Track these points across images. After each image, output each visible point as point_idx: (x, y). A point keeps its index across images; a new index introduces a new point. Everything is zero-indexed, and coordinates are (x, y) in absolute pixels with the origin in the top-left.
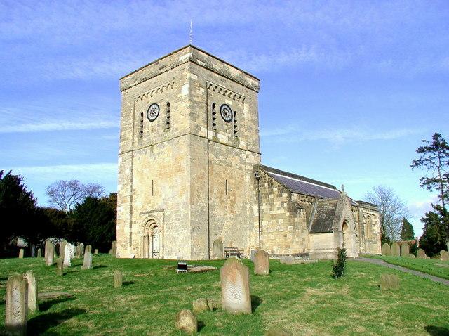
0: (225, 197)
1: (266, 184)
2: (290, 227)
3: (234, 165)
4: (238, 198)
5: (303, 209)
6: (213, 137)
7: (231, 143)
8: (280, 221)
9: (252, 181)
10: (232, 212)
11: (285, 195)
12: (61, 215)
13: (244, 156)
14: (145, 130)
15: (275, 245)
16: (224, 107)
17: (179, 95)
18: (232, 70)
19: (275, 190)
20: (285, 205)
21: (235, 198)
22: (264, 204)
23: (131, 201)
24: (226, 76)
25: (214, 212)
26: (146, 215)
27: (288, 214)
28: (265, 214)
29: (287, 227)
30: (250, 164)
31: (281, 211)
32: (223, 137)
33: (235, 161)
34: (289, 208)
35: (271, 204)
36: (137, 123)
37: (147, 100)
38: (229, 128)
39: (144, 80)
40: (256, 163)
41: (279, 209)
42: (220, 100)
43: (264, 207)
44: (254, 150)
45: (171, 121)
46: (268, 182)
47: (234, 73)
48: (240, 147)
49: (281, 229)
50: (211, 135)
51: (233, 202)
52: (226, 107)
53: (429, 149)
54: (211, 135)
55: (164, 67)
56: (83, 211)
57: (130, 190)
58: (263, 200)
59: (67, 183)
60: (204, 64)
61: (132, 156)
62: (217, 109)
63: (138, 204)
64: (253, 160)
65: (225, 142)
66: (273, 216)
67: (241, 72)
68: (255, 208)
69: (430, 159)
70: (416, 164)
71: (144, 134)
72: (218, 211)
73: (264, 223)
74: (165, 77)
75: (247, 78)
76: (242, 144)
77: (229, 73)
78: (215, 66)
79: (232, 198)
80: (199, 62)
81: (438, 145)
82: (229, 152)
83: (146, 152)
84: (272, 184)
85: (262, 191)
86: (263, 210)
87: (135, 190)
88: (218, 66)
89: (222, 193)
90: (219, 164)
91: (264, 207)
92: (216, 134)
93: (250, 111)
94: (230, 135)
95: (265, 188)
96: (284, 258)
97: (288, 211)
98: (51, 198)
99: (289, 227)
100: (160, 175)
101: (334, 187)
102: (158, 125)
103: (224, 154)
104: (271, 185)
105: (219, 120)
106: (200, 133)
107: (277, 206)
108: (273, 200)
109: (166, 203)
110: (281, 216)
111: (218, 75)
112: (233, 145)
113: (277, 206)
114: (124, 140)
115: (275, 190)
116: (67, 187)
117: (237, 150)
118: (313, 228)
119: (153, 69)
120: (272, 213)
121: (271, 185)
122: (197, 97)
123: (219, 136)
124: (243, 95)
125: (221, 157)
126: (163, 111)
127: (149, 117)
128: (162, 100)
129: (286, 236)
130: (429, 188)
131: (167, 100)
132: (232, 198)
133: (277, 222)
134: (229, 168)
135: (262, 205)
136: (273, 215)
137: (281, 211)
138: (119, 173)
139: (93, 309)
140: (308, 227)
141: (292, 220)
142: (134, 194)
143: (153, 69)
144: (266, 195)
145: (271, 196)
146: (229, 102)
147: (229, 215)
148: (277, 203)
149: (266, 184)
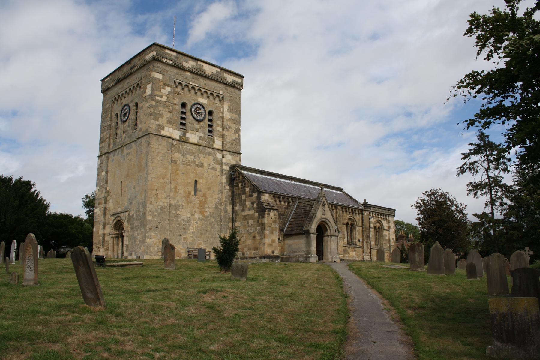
0: (193, 197)
1: (240, 184)
2: (259, 228)
3: (205, 164)
4: (210, 199)
5: (274, 210)
6: (180, 137)
7: (203, 143)
8: (251, 222)
9: (227, 181)
10: (202, 213)
11: (255, 195)
14: (119, 132)
15: (246, 247)
17: (144, 95)
18: (206, 67)
19: (247, 190)
20: (255, 205)
21: (206, 198)
22: (238, 205)
23: (105, 203)
24: (199, 74)
25: (178, 212)
26: (115, 217)
27: (257, 215)
28: (238, 215)
29: (256, 229)
30: (227, 164)
31: (251, 212)
32: (193, 137)
33: (207, 161)
34: (258, 208)
35: (243, 205)
36: (113, 124)
38: (201, 127)
40: (234, 163)
41: (250, 209)
42: (190, 98)
43: (237, 208)
44: (233, 150)
45: (138, 122)
46: (241, 182)
47: (209, 70)
48: (215, 146)
49: (251, 230)
50: (177, 134)
51: (203, 204)
53: (476, 152)
54: (177, 134)
55: (134, 66)
57: (104, 192)
58: (237, 201)
60: (171, 62)
61: (108, 159)
62: (188, 107)
63: (111, 205)
64: (230, 159)
65: (196, 141)
66: (246, 218)
67: (219, 70)
68: (229, 208)
70: (462, 170)
71: (119, 135)
72: (183, 211)
75: (226, 75)
76: (218, 144)
77: (204, 71)
78: (185, 64)
82: (202, 152)
83: (118, 153)
84: (245, 184)
85: (237, 192)
86: (237, 211)
87: (109, 192)
88: (190, 64)
89: (189, 193)
90: (186, 164)
92: (184, 134)
93: (230, 110)
94: (202, 135)
95: (238, 189)
96: (329, 251)
97: (257, 212)
99: (258, 228)
100: (128, 175)
101: (340, 189)
102: (129, 126)
103: (193, 154)
106: (163, 133)
107: (248, 206)
108: (245, 201)
109: (131, 203)
110: (251, 217)
111: (188, 74)
112: (206, 146)
113: (248, 206)
115: (247, 190)
117: (211, 150)
121: (244, 187)
122: (162, 97)
123: (188, 135)
124: (221, 93)
125: (190, 157)
126: (133, 108)
129: (254, 237)
131: (136, 100)
133: (248, 223)
134: (199, 168)
135: (236, 206)
136: (245, 216)
137: (251, 212)
139: (16, 323)
140: (282, 230)
141: (260, 220)
142: (108, 195)
144: (240, 195)
145: (244, 197)
146: (203, 100)
147: (197, 215)
148: (248, 204)
149: (240, 184)
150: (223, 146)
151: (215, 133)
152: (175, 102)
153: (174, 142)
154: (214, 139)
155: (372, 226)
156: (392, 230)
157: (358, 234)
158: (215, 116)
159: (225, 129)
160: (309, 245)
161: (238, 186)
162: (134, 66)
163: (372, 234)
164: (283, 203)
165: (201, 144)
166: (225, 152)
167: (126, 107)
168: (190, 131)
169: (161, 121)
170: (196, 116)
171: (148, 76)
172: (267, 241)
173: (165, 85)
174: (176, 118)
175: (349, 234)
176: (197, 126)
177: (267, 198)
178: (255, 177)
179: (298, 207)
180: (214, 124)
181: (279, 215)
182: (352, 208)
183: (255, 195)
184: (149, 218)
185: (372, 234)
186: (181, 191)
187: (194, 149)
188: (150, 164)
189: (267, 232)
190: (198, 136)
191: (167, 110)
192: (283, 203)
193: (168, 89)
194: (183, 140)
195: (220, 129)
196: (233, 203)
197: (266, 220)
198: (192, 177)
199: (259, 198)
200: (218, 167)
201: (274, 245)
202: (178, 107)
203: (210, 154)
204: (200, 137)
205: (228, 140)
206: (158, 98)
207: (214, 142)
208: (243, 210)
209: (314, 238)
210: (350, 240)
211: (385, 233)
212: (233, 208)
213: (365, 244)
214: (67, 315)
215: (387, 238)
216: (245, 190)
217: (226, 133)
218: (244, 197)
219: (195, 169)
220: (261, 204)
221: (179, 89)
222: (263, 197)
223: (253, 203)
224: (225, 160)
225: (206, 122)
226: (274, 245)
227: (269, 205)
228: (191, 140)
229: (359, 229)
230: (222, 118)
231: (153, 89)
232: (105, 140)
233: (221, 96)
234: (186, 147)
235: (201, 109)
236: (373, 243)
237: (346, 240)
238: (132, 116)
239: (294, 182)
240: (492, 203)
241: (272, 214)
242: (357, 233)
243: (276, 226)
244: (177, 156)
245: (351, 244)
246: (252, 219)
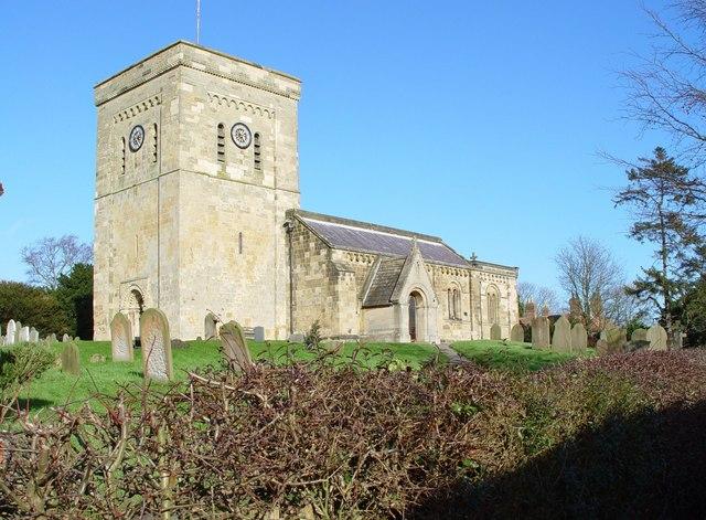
1: (301, 237)
3: (253, 209)
7: (249, 179)
8: (318, 289)
11: (324, 252)
12: (38, 292)
13: (270, 197)
16: (237, 127)
21: (255, 258)
34: (328, 270)
35: (307, 266)
37: (129, 121)
39: (125, 91)
41: (316, 272)
43: (298, 270)
44: (289, 188)
48: (264, 184)
50: (214, 168)
52: (242, 127)
53: (648, 174)
55: (149, 72)
56: (635, 338)
59: (57, 241)
60: (203, 67)
62: (227, 130)
66: (311, 284)
68: (286, 271)
69: (643, 192)
73: (299, 293)
74: (149, 89)
78: (222, 69)
79: (250, 257)
80: (194, 65)
81: (664, 172)
91: (298, 270)
92: (224, 168)
94: (246, 168)
98: (30, 267)
101: (436, 240)
103: (235, 195)
104: (307, 238)
105: (229, 146)
106: (196, 168)
108: (309, 260)
111: (226, 81)
114: (101, 178)
115: (312, 245)
116: (57, 249)
117: (258, 189)
118: (370, 298)
119: (136, 74)
120: (308, 278)
121: (307, 238)
122: (192, 117)
123: (228, 169)
125: (232, 200)
127: (132, 144)
128: (147, 121)
130: (639, 239)
132: (250, 257)
133: (314, 291)
136: (309, 282)
137: (320, 276)
138: (96, 226)
140: (360, 298)
143: (136, 74)
144: (301, 253)
145: (307, 255)
146: (245, 119)
147: (244, 282)
148: (314, 265)
150: (275, 183)
152: (210, 123)
153: (211, 180)
155: (483, 292)
156: (514, 298)
157: (464, 304)
158: (262, 140)
160: (398, 319)
161: (298, 239)
162: (149, 72)
163: (484, 305)
164: (361, 262)
166: (278, 192)
167: (138, 129)
169: (195, 152)
170: (238, 143)
171: (172, 89)
172: (341, 315)
173: (198, 100)
175: (451, 305)
177: (340, 257)
178: (321, 226)
179: (382, 268)
181: (357, 279)
183: (324, 252)
184: (182, 287)
185: (484, 305)
186: (222, 249)
187: (237, 187)
188: (181, 212)
189: (341, 304)
192: (361, 262)
193: (201, 106)
194: (223, 176)
195: (270, 158)
196: (291, 263)
197: (340, 287)
198: (237, 228)
199: (329, 255)
200: (270, 212)
201: (351, 320)
202: (215, 130)
203: (258, 195)
205: (282, 173)
206: (188, 119)
208: (307, 274)
209: (405, 309)
210: (452, 312)
211: (503, 302)
212: (291, 270)
213: (474, 319)
214: (138, 440)
215: (506, 310)
216: (308, 246)
217: (278, 164)
218: (307, 255)
219: (239, 217)
220: (333, 265)
221: (214, 104)
222: (334, 256)
223: (320, 264)
224: (278, 203)
225: (252, 147)
226: (351, 320)
227: (343, 266)
229: (465, 297)
230: (274, 142)
231: (179, 106)
234: (226, 186)
236: (485, 317)
237: (447, 314)
238: (149, 143)
239: (372, 231)
240: (664, 253)
241: (347, 278)
242: (463, 303)
243: (354, 295)
244: (215, 199)
245: (454, 318)
246: (319, 285)
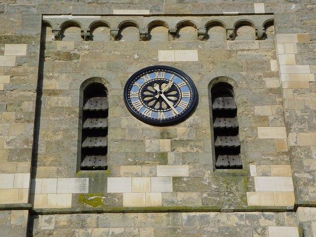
42: (112, 60)
62: (115, 90)
92: (99, 186)
94: (183, 171)
124: (259, 8)
150: (297, 192)
151: (249, 152)
154: (247, 175)
159: (295, 126)
165: (181, 205)
168: (124, 169)
174: (59, 137)
176: (154, 141)
180: (242, 121)
182: (217, 114)
190: (165, 179)
191: (12, 115)
204: (176, 180)
207: (249, 186)
228: (128, 202)
232: (168, 82)
233: (259, 22)
235: (160, 82)
